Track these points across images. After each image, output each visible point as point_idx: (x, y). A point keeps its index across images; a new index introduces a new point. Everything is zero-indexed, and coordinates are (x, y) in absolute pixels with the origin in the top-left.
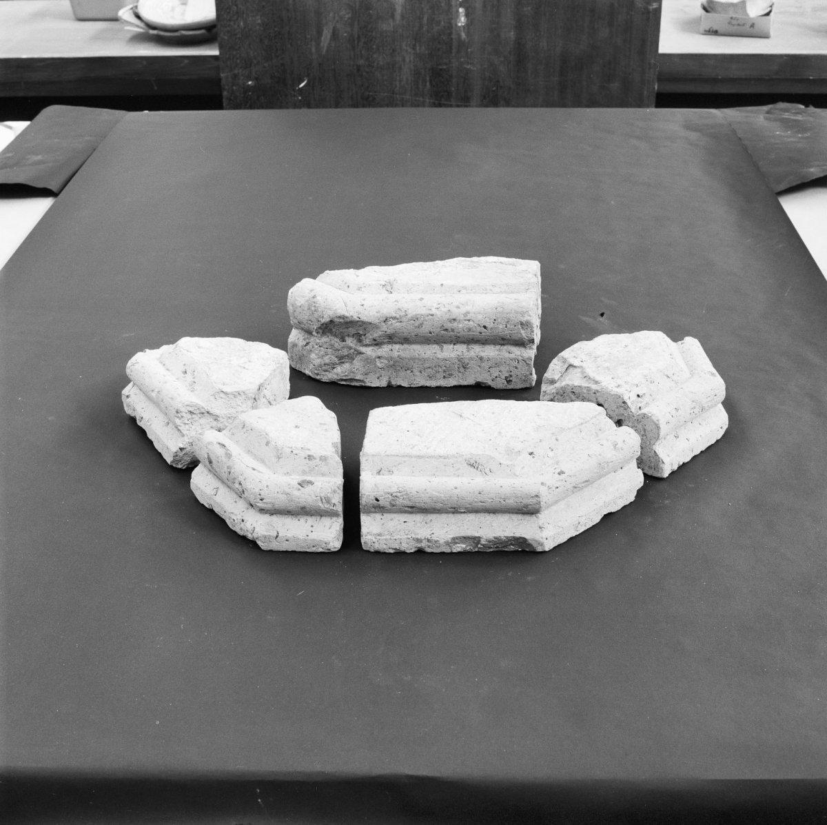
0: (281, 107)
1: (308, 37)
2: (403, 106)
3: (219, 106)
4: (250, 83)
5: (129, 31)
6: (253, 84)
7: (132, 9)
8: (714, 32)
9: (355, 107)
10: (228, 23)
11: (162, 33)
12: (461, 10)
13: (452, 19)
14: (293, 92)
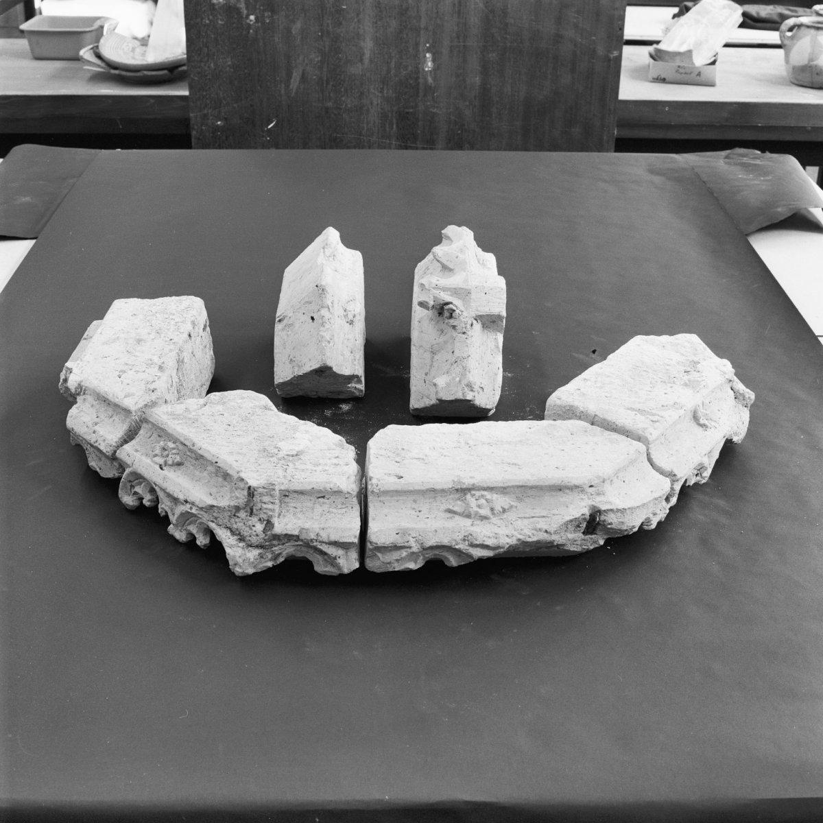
0: (249, 147)
2: (369, 148)
3: (188, 145)
4: (219, 123)
6: (223, 124)
7: (92, 49)
8: (662, 80)
9: (322, 148)
10: (199, 65)
11: (124, 73)
12: (428, 55)
13: (419, 64)
14: (261, 133)
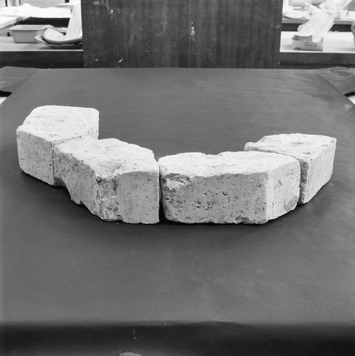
1: (123, 39)
4: (97, 60)
5: (39, 47)
12: (192, 28)
13: (188, 32)
14: (116, 65)
